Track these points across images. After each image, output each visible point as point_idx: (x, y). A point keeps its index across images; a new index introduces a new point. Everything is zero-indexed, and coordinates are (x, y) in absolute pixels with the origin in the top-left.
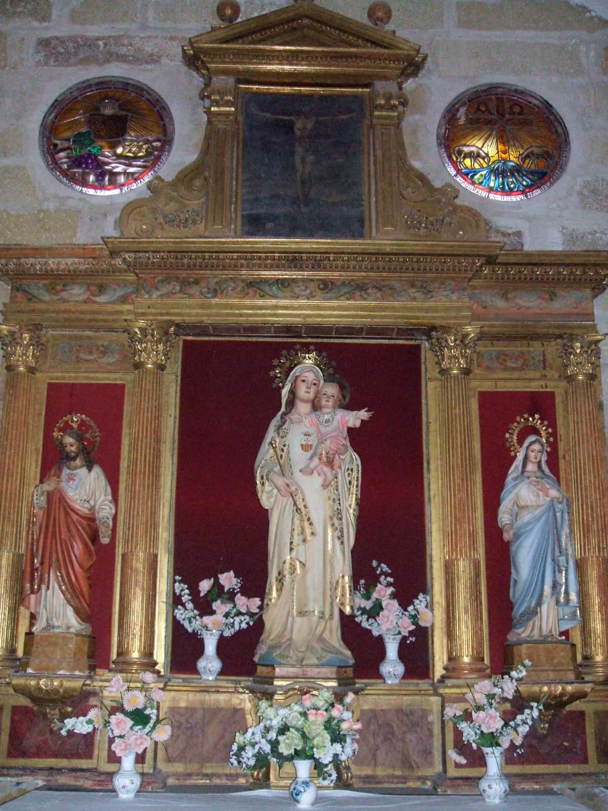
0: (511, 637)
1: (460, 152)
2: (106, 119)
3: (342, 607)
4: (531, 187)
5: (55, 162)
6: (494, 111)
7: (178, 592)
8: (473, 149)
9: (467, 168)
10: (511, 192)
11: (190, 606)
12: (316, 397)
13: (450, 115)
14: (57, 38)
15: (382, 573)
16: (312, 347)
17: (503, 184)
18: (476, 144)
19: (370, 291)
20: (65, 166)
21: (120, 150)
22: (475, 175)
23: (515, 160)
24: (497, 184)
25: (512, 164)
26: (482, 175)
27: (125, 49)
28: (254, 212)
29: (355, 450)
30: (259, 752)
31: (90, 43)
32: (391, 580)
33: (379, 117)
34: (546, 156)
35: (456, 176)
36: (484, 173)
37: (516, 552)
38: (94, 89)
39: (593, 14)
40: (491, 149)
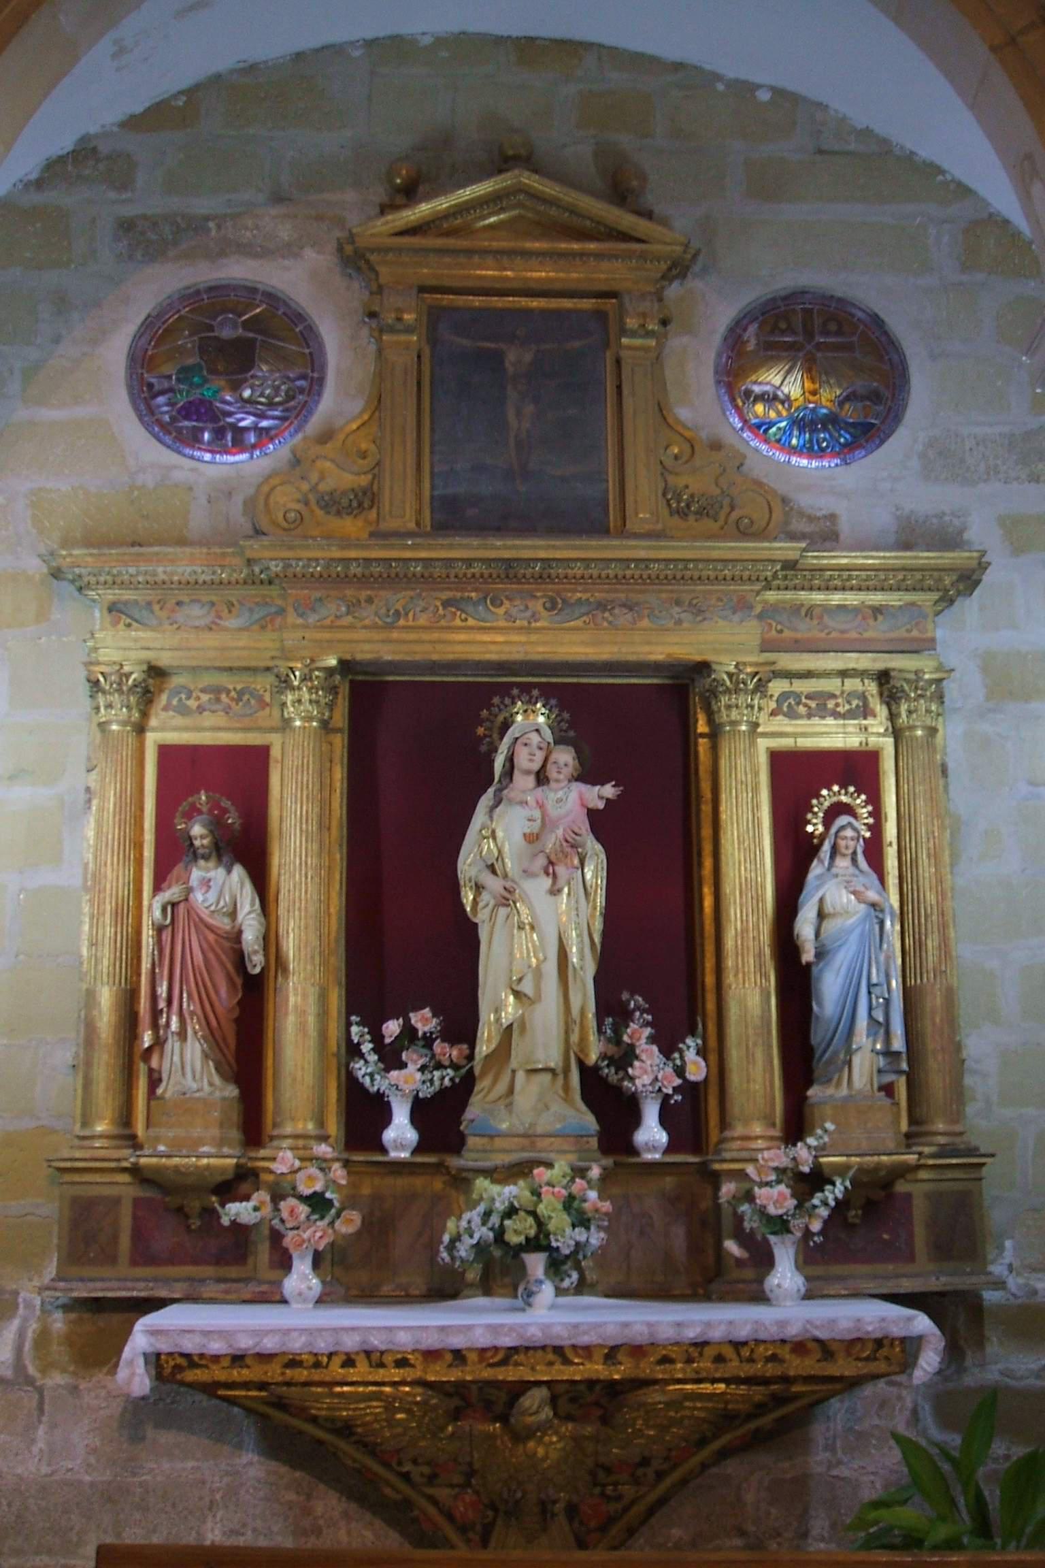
0: (813, 1092)
1: (748, 393)
2: (224, 347)
3: (582, 1056)
4: (850, 447)
5: (151, 412)
6: (800, 329)
7: (356, 1040)
8: (767, 388)
9: (757, 417)
10: (821, 453)
11: (373, 1058)
12: (544, 766)
13: (734, 338)
14: (145, 217)
15: (637, 1008)
16: (535, 692)
17: (811, 440)
18: (772, 378)
19: (617, 611)
20: (167, 418)
21: (247, 393)
22: (770, 428)
23: (828, 404)
24: (802, 442)
25: (824, 411)
26: (779, 429)
27: (248, 234)
28: (450, 491)
29: (598, 839)
30: (478, 1243)
31: (197, 225)
32: (649, 1018)
33: (629, 348)
34: (875, 397)
35: (742, 429)
36: (783, 424)
37: (819, 979)
38: (205, 297)
39: (949, 177)
40: (794, 388)
